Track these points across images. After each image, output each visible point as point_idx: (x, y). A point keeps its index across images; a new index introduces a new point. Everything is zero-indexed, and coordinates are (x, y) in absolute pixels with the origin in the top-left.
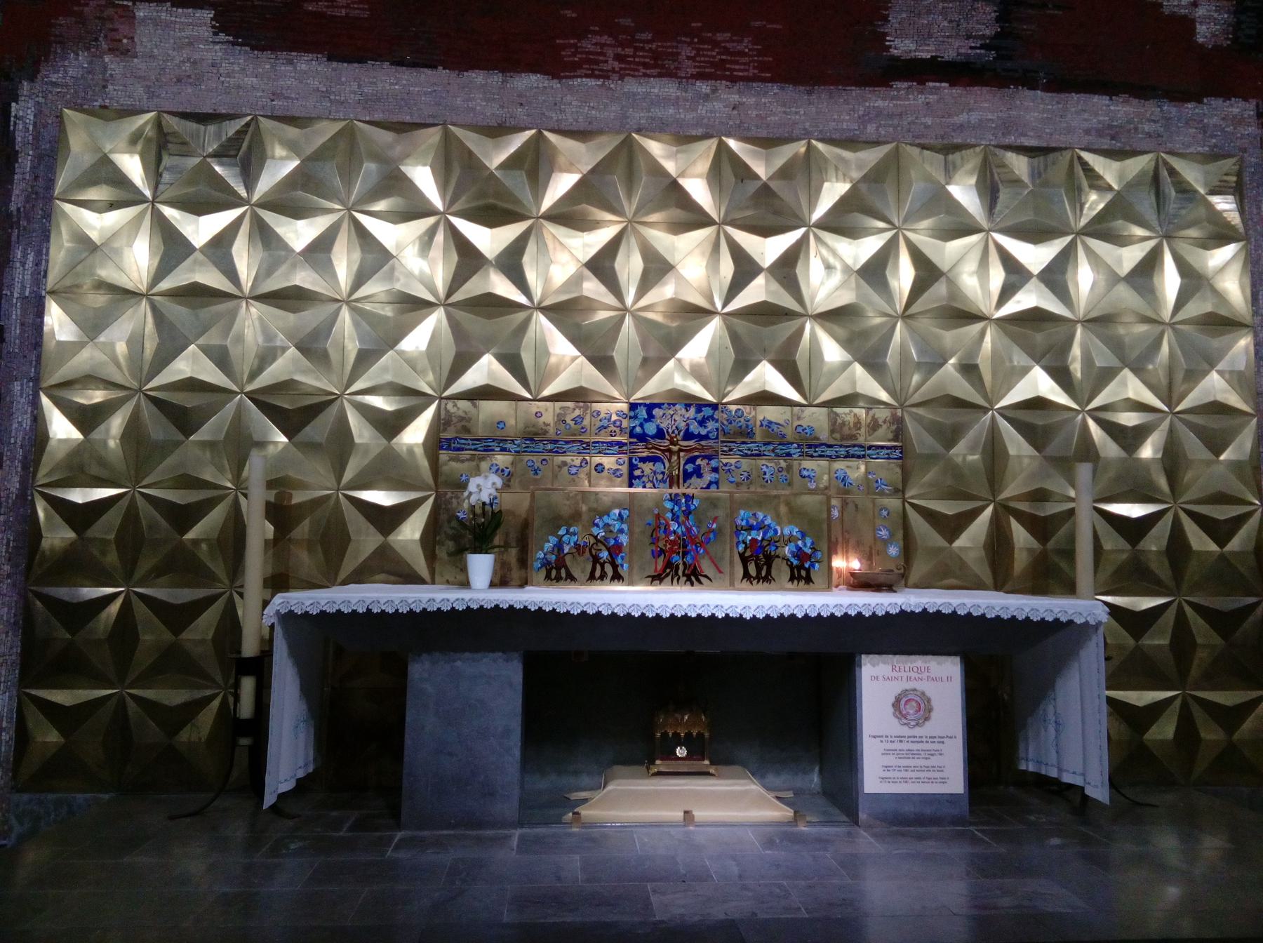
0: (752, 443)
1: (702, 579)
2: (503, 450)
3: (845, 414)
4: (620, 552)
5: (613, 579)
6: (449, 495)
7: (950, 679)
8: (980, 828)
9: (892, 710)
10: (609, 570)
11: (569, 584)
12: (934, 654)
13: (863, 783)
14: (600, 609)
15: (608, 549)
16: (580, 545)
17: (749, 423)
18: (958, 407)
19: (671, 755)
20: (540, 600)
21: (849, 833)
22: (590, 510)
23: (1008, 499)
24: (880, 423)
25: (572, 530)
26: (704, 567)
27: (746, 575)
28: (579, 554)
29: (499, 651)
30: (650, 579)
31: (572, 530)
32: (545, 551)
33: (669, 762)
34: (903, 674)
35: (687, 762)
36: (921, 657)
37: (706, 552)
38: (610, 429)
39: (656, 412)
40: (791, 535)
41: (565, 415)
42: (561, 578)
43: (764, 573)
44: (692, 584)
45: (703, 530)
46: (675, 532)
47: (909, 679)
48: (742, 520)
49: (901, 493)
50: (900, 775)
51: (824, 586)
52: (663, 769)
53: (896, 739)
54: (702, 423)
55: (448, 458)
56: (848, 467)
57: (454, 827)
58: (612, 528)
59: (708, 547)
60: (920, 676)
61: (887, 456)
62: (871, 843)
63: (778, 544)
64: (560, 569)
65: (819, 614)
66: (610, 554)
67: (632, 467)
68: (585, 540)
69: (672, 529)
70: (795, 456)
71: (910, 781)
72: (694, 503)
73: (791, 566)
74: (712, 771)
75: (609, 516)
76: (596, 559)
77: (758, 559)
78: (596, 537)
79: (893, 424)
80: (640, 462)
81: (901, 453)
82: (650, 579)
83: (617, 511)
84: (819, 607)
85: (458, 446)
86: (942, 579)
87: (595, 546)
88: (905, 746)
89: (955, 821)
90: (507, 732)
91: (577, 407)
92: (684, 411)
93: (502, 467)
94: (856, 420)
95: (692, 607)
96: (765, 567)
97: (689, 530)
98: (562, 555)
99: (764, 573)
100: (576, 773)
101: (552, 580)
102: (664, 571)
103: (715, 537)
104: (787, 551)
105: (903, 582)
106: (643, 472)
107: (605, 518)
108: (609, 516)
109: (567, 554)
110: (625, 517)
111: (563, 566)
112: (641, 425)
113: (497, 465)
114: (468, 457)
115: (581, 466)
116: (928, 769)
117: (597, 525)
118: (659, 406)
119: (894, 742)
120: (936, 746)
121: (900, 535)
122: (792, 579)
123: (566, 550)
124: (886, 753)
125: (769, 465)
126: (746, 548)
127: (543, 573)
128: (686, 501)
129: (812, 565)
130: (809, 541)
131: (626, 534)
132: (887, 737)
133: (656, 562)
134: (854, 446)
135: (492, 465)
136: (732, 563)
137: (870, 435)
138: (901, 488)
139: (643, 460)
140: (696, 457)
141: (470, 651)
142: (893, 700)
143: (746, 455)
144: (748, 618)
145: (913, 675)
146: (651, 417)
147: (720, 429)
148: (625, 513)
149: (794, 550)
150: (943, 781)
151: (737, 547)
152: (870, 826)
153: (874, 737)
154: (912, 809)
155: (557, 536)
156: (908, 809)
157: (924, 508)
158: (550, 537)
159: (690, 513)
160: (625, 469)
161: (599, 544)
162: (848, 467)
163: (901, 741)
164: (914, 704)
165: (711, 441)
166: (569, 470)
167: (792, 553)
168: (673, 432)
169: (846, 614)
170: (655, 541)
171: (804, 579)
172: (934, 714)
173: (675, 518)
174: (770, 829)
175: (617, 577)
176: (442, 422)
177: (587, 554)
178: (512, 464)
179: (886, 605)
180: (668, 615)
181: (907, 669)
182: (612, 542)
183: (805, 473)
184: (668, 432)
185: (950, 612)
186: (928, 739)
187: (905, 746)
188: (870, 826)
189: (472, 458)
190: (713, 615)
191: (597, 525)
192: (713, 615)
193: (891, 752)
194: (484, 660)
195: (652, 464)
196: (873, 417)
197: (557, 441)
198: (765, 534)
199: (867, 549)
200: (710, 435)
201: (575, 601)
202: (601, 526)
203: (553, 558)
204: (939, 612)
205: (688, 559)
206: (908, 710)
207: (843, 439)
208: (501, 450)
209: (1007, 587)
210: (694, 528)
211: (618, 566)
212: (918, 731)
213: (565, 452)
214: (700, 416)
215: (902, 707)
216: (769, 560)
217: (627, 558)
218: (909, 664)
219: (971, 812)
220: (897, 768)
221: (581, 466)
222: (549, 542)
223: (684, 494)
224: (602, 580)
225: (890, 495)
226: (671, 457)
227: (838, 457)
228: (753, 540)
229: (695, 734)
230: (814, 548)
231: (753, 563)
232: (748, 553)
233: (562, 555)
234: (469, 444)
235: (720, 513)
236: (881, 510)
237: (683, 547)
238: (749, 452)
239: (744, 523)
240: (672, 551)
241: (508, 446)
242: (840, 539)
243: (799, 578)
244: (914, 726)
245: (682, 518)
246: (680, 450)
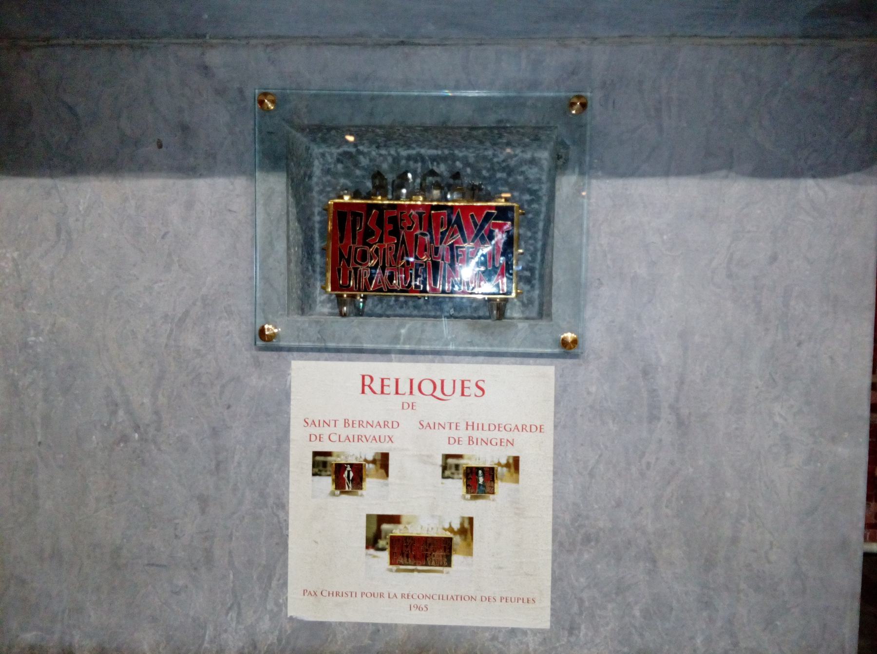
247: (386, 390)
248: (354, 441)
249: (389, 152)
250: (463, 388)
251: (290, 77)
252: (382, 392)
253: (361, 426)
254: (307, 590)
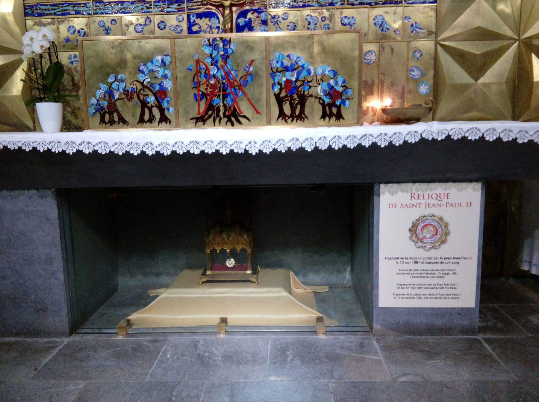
1: (242, 119)
2: (78, 13)
4: (166, 96)
5: (161, 121)
8: (489, 336)
9: (408, 234)
10: (156, 112)
11: (122, 127)
12: (455, 181)
13: (377, 299)
14: (96, 149)
15: (155, 94)
16: (128, 91)
20: (33, 140)
21: (362, 345)
22: (135, 57)
23: (530, 38)
25: (119, 77)
26: (242, 109)
27: (282, 114)
28: (128, 99)
29: (33, 189)
30: (194, 121)
31: (119, 77)
32: (98, 98)
34: (423, 202)
36: (441, 184)
37: (244, 93)
40: (324, 75)
42: (114, 122)
43: (297, 112)
44: (233, 125)
45: (241, 73)
46: (214, 76)
47: (427, 205)
48: (277, 62)
49: (434, 35)
51: (353, 122)
53: (411, 261)
55: (33, 23)
56: (386, 13)
57: (17, 335)
58: (156, 74)
59: (246, 89)
60: (439, 202)
63: (311, 84)
64: (113, 113)
65: (330, 147)
66: (156, 99)
67: (190, 25)
68: (132, 86)
69: (211, 73)
71: (423, 297)
72: (232, 47)
73: (323, 105)
74: (253, 280)
75: (152, 62)
76: (144, 104)
77: (292, 98)
78: (142, 83)
80: (197, 18)
82: (194, 121)
83: (159, 58)
84: (329, 139)
85: (40, 11)
86: (465, 113)
87: (142, 91)
88: (420, 266)
90: (49, 260)
93: (78, 28)
95: (195, 143)
96: (299, 106)
97: (227, 74)
98: (113, 101)
99: (297, 112)
100: (158, 275)
101: (106, 124)
102: (206, 112)
103: (252, 79)
104: (319, 90)
105: (431, 115)
106: (200, 27)
107: (149, 64)
108: (152, 62)
109: (118, 99)
110: (167, 63)
113: (74, 27)
114: (49, 20)
115: (146, 24)
117: (142, 72)
119: (409, 263)
120: (451, 266)
121: (431, 74)
122: (324, 117)
123: (117, 96)
124: (401, 272)
125: (313, 15)
126: (281, 89)
127: (98, 117)
128: (223, 46)
129: (343, 102)
130: (340, 80)
131: (170, 80)
132: (402, 258)
135: (70, 27)
136: (268, 103)
138: (434, 30)
140: (247, 11)
141: (7, 189)
142: (410, 225)
144: (254, 154)
145: (431, 201)
148: (168, 60)
150: (456, 297)
151: (273, 89)
153: (390, 259)
154: (424, 321)
155: (107, 83)
156: (421, 320)
157: (454, 49)
158: (101, 85)
159: (228, 57)
160: (184, 26)
161: (146, 90)
162: (386, 13)
163: (416, 263)
164: (431, 228)
166: (135, 28)
167: (324, 91)
169: (360, 145)
171: (336, 116)
172: (449, 238)
173: (214, 63)
174: (290, 338)
175: (164, 119)
177: (135, 99)
178: (87, 25)
179: (404, 134)
180: (169, 153)
181: (426, 196)
182: (158, 88)
183: (346, 21)
185: (477, 138)
187: (420, 266)
189: (52, 23)
190: (217, 151)
191: (142, 72)
192: (217, 151)
193: (406, 272)
194: (21, 197)
195: (208, 19)
198: (299, 74)
199: (400, 89)
201: (69, 140)
203: (106, 103)
204: (464, 138)
205: (229, 102)
206: (425, 234)
208: (76, 13)
209: (524, 117)
210: (232, 72)
211: (164, 109)
212: (433, 253)
215: (419, 232)
216: (303, 99)
217: (172, 102)
218: (428, 192)
220: (411, 286)
221: (146, 24)
222: (100, 89)
223: (221, 39)
224: (151, 122)
228: (288, 81)
229: (238, 250)
230: (345, 86)
231: (288, 103)
232: (283, 94)
233: (113, 101)
234: (49, 10)
235: (256, 56)
236: (415, 52)
239: (279, 65)
240: (213, 94)
241: (81, 9)
242: (376, 82)
243: (331, 115)
244: (430, 248)
245: (220, 63)
247: (420, 198)
248: (410, 207)
249: (227, 7)
250: (447, 196)
251: (43, 143)
252: (418, 199)
253: (413, 198)
254: (449, 203)
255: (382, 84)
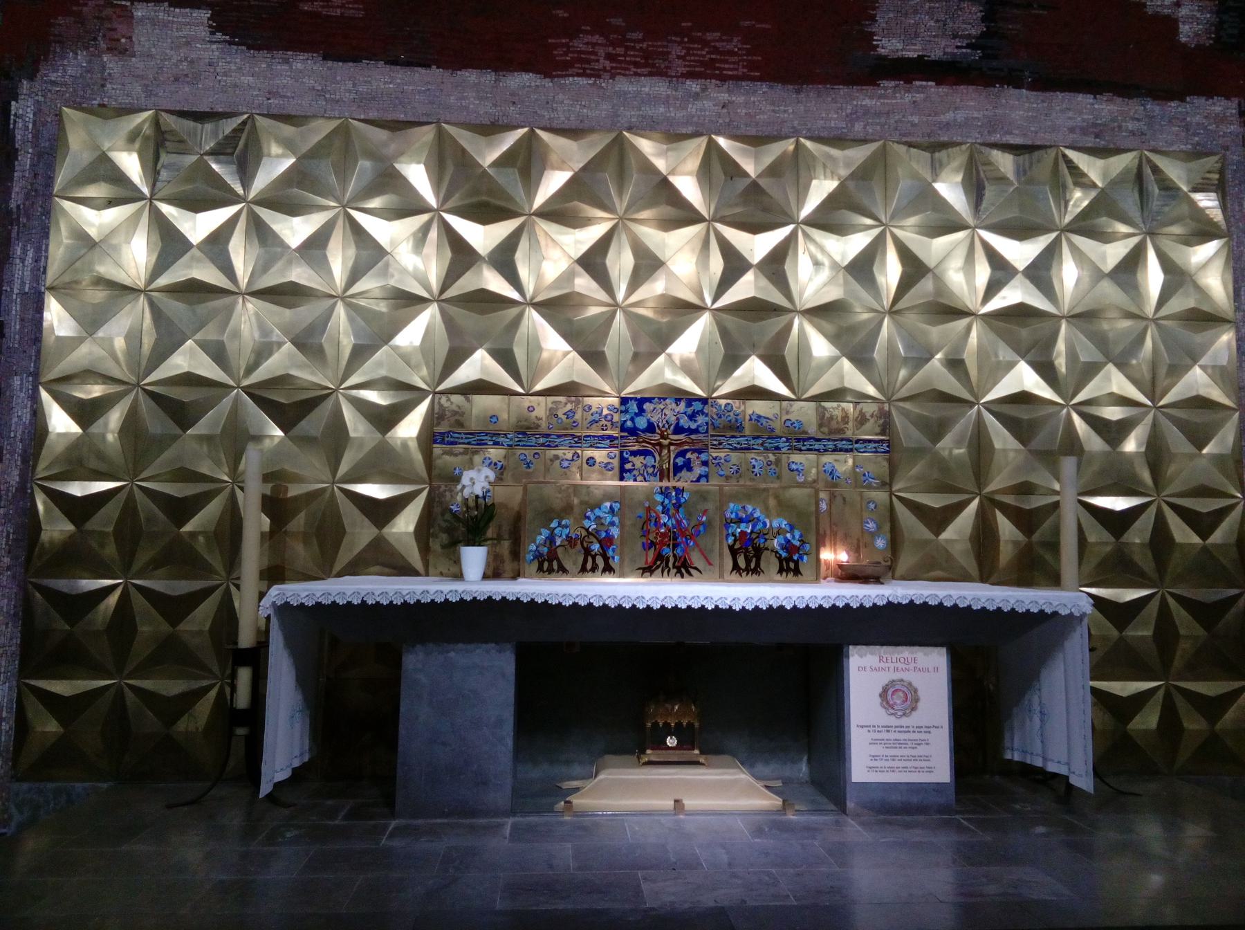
0: (741, 436)
1: (692, 571)
2: (496, 443)
3: (833, 408)
4: (612, 544)
5: (604, 571)
6: (443, 488)
7: (936, 669)
8: (966, 816)
9: (879, 700)
10: (600, 562)
11: (561, 576)
12: (920, 645)
13: (850, 772)
14: (591, 601)
15: (600, 542)
16: (571, 538)
17: (738, 417)
18: (944, 401)
19: (661, 745)
20: (532, 592)
22: (582, 503)
23: (993, 492)
24: (868, 417)
25: (563, 523)
26: (694, 559)
27: (736, 567)
28: (571, 546)
29: (492, 642)
30: (641, 571)
31: (563, 523)
32: (537, 543)
33: (660, 752)
35: (677, 752)
36: (908, 647)
38: (601, 423)
39: (647, 406)
40: (780, 528)
41: (557, 409)
42: (553, 570)
43: (753, 565)
44: (682, 576)
45: (693, 523)
46: (665, 524)
47: (896, 669)
48: (732, 513)
49: (888, 486)
50: (887, 764)
51: (812, 578)
52: (653, 759)
53: (883, 729)
54: (692, 417)
55: (441, 452)
56: (836, 460)
57: (448, 816)
58: (603, 521)
59: (698, 539)
60: (907, 667)
61: (874, 450)
62: (858, 831)
63: (767, 537)
64: (552, 561)
65: (807, 606)
66: (601, 546)
67: (623, 461)
68: (576, 532)
69: (662, 522)
70: (784, 450)
71: (897, 770)
72: (685, 496)
73: (780, 559)
74: (702, 760)
75: (600, 508)
76: (587, 552)
77: (747, 551)
78: (587, 530)
79: (880, 418)
80: (631, 455)
81: (888, 446)
82: (641, 571)
83: (608, 504)
84: (807, 598)
85: (452, 440)
86: (929, 571)
87: (586, 538)
88: (892, 736)
89: (942, 810)
90: (500, 722)
91: (569, 401)
92: (674, 405)
93: (494, 460)
94: (844, 415)
95: (682, 598)
96: (754, 560)
97: (679, 522)
98: (554, 547)
99: (753, 565)
100: (568, 762)
101: (544, 572)
102: (654, 563)
103: (705, 529)
104: (775, 543)
105: (890, 574)
106: (634, 465)
107: (597, 511)
108: (600, 508)
109: (559, 546)
110: (616, 509)
111: (555, 558)
112: (632, 419)
113: (490, 459)
114: (461, 450)
115: (573, 460)
116: (915, 758)
117: (589, 518)
118: (650, 400)
119: (881, 731)
120: (923, 736)
121: (887, 527)
122: (781, 571)
123: (558, 542)
124: (874, 742)
125: (758, 458)
126: (735, 541)
127: (535, 565)
129: (801, 557)
130: (797, 534)
131: (617, 527)
132: (874, 726)
133: (647, 555)
134: (842, 440)
135: (485, 459)
136: (721, 555)
137: (857, 429)
138: (888, 481)
139: (634, 453)
140: (687, 451)
141: (464, 642)
142: (880, 690)
143: (736, 449)
144: (738, 610)
145: (900, 665)
146: (641, 411)
147: (710, 423)
148: (616, 506)
149: (783, 542)
150: (930, 770)
151: (727, 539)
152: (858, 815)
153: (862, 727)
154: (899, 798)
155: (549, 529)
156: (895, 798)
157: (911, 501)
158: (542, 530)
159: (680, 506)
160: (616, 463)
161: (591, 537)
162: (836, 460)
163: (888, 731)
164: (901, 694)
165: (700, 435)
166: (561, 464)
167: (781, 545)
168: (664, 426)
169: (834, 605)
170: (646, 533)
171: (793, 571)
172: (920, 705)
173: (665, 511)
175: (608, 569)
176: (436, 416)
177: (579, 546)
178: (505, 457)
179: (873, 597)
180: (659, 607)
181: (894, 660)
182: (603, 535)
183: (794, 467)
184: (658, 426)
185: (937, 603)
186: (915, 729)
187: (892, 736)
188: (858, 815)
189: (466, 452)
190: (703, 606)
191: (589, 518)
192: (703, 606)
193: (878, 742)
194: (478, 651)
195: (642, 457)
196: (861, 411)
197: (549, 435)
198: (754, 526)
199: (855, 542)
200: (700, 429)
201: (567, 592)
202: (592, 519)
203: (545, 550)
205: (679, 551)
206: (895, 700)
207: (831, 433)
208: (494, 444)
210: (684, 521)
211: (609, 558)
212: (905, 721)
213: (557, 446)
214: (690, 411)
215: (889, 697)
216: (758, 552)
217: (618, 551)
218: (896, 655)
219: (957, 800)
220: (884, 758)
221: (573, 460)
222: (541, 534)
223: (674, 487)
224: (594, 572)
225: (878, 488)
226: (661, 451)
227: (826, 450)
228: (743, 533)
229: (685, 724)
230: (802, 540)
231: (742, 555)
232: (737, 546)
233: (554, 547)
234: (462, 438)
235: (710, 506)
236: (869, 503)
237: (673, 540)
238: (739, 446)
239: (733, 516)
240: (662, 543)
241: (501, 439)
242: (828, 532)
243: (788, 570)
244: (901, 716)
245: (672, 511)
246: (671, 444)
255: (835, 534)
